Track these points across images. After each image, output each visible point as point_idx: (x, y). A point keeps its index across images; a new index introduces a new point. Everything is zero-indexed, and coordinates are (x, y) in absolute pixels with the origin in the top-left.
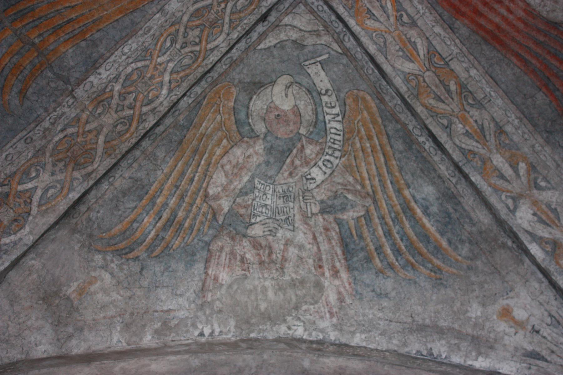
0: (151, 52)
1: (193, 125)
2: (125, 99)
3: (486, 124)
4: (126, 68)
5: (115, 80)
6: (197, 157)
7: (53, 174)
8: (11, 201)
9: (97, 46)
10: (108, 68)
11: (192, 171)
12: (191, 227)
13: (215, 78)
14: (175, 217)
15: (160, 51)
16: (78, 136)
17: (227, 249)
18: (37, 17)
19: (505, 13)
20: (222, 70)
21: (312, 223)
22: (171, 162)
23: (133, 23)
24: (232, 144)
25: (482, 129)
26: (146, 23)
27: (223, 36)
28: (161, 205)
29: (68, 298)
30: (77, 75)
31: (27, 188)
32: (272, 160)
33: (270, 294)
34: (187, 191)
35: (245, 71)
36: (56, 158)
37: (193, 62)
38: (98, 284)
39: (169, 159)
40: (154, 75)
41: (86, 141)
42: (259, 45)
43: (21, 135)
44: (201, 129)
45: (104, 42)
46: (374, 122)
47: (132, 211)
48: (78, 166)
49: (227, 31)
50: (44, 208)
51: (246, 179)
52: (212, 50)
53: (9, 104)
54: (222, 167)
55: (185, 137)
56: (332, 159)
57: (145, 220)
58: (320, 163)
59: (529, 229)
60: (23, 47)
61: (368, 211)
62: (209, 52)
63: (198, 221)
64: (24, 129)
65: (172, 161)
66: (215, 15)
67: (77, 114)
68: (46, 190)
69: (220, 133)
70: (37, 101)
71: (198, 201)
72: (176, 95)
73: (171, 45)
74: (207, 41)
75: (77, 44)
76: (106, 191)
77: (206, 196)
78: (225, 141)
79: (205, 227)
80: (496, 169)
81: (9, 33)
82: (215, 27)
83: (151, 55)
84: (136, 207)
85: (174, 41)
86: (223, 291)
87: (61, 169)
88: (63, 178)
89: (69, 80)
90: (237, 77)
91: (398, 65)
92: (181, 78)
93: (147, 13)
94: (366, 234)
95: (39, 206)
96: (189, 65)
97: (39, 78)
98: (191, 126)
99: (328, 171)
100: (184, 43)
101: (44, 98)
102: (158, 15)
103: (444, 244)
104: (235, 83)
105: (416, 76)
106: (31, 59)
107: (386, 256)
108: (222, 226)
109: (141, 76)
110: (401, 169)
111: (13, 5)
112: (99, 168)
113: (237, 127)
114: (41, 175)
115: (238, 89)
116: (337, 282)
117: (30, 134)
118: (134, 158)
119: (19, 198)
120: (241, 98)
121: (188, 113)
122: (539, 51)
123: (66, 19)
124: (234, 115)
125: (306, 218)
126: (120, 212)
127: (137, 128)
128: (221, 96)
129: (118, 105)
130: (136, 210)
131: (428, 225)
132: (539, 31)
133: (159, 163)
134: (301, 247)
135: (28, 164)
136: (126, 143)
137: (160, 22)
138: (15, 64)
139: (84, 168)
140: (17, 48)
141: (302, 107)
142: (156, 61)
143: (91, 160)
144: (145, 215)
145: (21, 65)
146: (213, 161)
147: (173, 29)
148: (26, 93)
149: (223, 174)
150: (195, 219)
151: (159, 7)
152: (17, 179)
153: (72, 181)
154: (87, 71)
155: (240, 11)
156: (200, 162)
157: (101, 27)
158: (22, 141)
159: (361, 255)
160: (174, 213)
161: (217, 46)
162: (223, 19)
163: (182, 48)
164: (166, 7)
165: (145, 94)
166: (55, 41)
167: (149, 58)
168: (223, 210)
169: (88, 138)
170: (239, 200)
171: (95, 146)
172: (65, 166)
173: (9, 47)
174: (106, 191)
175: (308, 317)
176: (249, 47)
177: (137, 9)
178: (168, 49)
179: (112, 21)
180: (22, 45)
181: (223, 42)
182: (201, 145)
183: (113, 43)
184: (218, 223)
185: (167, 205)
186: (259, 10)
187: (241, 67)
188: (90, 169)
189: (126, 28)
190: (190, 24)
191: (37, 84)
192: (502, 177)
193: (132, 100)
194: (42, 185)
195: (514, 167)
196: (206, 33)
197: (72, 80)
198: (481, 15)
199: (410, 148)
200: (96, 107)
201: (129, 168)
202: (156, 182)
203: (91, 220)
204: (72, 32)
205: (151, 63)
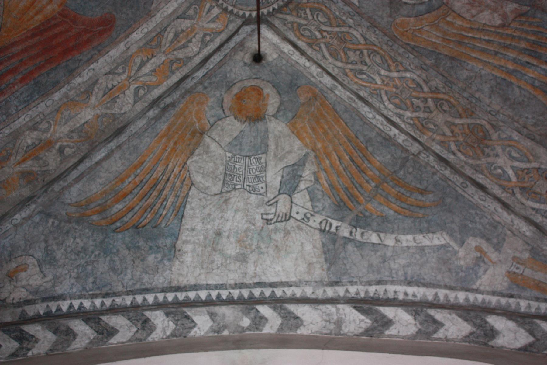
0: (373, 90)
1: (434, 50)
2: (418, 107)
4: (390, 110)
5: (402, 117)
6: (466, 41)
7: (497, 155)
8: (528, 184)
9: (370, 138)
10: (388, 129)
11: (479, 43)
12: (535, 33)
13: (388, 39)
14: (526, 49)
15: (371, 83)
16: (458, 141)
18: (352, 185)
20: (381, 33)
22: (472, 63)
23: (346, 110)
24: (450, 12)
26: (344, 101)
27: (351, 31)
28: (515, 65)
30: (399, 153)
31: (514, 174)
34: (500, 44)
35: (380, 13)
36: (481, 155)
37: (378, 53)
39: (469, 66)
40: (393, 85)
41: (462, 134)
42: (355, 4)
43: (460, 191)
44: (438, 42)
45: (366, 133)
47: (523, 89)
48: (486, 136)
49: (348, 28)
50: (531, 158)
52: (366, 39)
53: (434, 201)
54: (473, 16)
55: (446, 55)
57: (532, 75)
60: (380, 194)
62: (368, 42)
63: (529, 29)
64: (454, 189)
65: (470, 63)
66: (334, 39)
67: (437, 144)
68: (513, 158)
69: (441, 25)
70: (427, 181)
71: (509, 32)
72: (410, 65)
73: (365, 74)
74: (357, 45)
75: (371, 153)
76: (506, 116)
77: (503, 26)
78: (448, 19)
79: (534, 21)
81: (369, 206)
82: (345, 39)
83: (375, 89)
84: (519, 87)
85: (361, 72)
87: (492, 150)
88: (499, 147)
89: (404, 158)
90: (385, 20)
92: (394, 62)
93: (336, 100)
95: (529, 161)
96: (381, 57)
97: (406, 181)
98: (435, 52)
100: (362, 63)
101: (423, 176)
102: (337, 92)
104: (392, 20)
106: (390, 188)
109: (396, 96)
111: (345, 204)
112: (486, 119)
113: (434, 10)
114: (499, 165)
115: (397, 17)
117: (458, 184)
118: (470, 97)
119: (524, 179)
120: (405, 13)
121: (424, 57)
123: (351, 163)
124: (422, 15)
126: (525, 99)
127: (444, 93)
128: (405, 30)
129: (424, 112)
130: (522, 86)
133: (474, 74)
135: (490, 176)
136: (460, 100)
137: (342, 91)
138: (397, 199)
139: (487, 131)
140: (382, 198)
142: (380, 85)
143: (480, 127)
144: (526, 77)
145: (397, 195)
146: (468, 26)
147: (350, 74)
148: (422, 189)
149: (481, 14)
150: (527, 32)
151: (329, 92)
152: (506, 183)
153: (502, 139)
154: (394, 145)
155: (329, 19)
156: (471, 37)
157: (354, 136)
158: (466, 190)
160: (523, 52)
161: (362, 36)
162: (337, 32)
163: (366, 65)
164: (328, 86)
165: (411, 90)
166: (371, 170)
167: (378, 91)
168: (516, 8)
169: (459, 132)
171: (466, 126)
172: (488, 147)
173: (382, 205)
174: (506, 116)
176: (357, 13)
177: (333, 108)
178: (368, 76)
179: (346, 127)
180: (378, 195)
181: (357, 30)
182: (453, 39)
183: (366, 126)
184: (529, 10)
185: (514, 59)
186: (326, 3)
187: (376, 17)
188: (488, 127)
189: (351, 116)
190: (344, 60)
191: (412, 181)
193: (419, 101)
194: (509, 163)
196: (351, 46)
197: (404, 155)
200: (429, 129)
201: (480, 101)
202: (493, 73)
203: (535, 123)
204: (361, 158)
205: (383, 89)
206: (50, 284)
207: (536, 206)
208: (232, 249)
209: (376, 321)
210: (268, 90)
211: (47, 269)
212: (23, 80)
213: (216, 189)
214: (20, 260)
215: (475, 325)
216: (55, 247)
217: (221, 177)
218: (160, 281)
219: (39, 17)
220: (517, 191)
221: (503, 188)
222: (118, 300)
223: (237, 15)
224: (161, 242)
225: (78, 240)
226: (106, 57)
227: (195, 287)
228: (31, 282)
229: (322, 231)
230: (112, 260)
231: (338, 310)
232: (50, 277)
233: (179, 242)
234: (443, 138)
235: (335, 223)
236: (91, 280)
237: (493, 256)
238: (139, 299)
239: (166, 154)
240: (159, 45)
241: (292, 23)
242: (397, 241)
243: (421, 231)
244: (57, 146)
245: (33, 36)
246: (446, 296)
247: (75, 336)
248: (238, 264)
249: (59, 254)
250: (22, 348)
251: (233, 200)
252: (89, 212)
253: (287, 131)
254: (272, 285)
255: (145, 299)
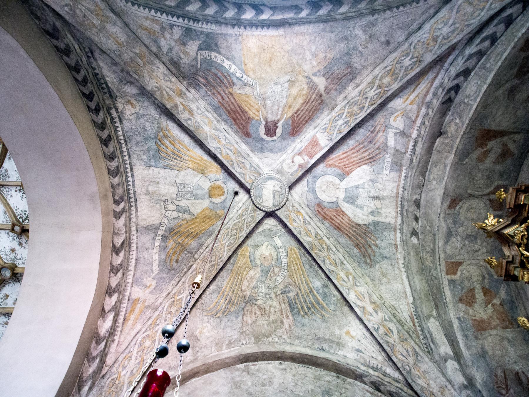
3: (337, 261)
12: (237, 303)
17: (250, 310)
19: (342, 220)
21: (278, 298)
25: (336, 262)
27: (244, 231)
29: (196, 336)
32: (263, 275)
33: (265, 326)
38: (206, 329)
46: (298, 258)
51: (255, 283)
56: (284, 273)
58: (280, 275)
59: (354, 302)
61: (297, 293)
80: (341, 277)
85: (227, 235)
86: (249, 326)
91: (305, 238)
94: (298, 302)
99: (283, 278)
103: (325, 305)
105: (312, 242)
107: (305, 310)
108: (247, 302)
110: (308, 276)
116: (288, 321)
122: (354, 234)
125: (276, 296)
131: (319, 298)
132: (353, 226)
134: (275, 307)
141: (272, 254)
159: (296, 310)
170: (253, 291)
175: (279, 334)
192: (344, 281)
195: (348, 277)
198: (333, 220)
199: (311, 267)
206: (127, 118)
207: (166, 308)
208: (151, 189)
209: (118, 249)
210: (223, 198)
211: (134, 116)
212: (220, 102)
213: (178, 181)
214: (137, 104)
215: (115, 288)
216: (145, 118)
217: (184, 182)
218: (134, 161)
219: (247, 109)
220: (173, 299)
221: (175, 294)
222: (124, 145)
223: (251, 187)
224: (153, 160)
225: (150, 128)
226: (234, 134)
227: (133, 176)
228: (127, 110)
229: (160, 224)
230: (142, 142)
231: (123, 234)
232: (131, 118)
233: (153, 168)
234: (198, 268)
235: (164, 228)
236: (131, 134)
237: (148, 291)
238: (126, 154)
239: (193, 160)
240: (238, 156)
241: (248, 208)
242: (155, 253)
243: (159, 262)
244: (191, 118)
245: (239, 107)
246: (130, 275)
247: (102, 131)
248: (145, 191)
249: (142, 120)
250: (92, 110)
251: (173, 187)
252: (164, 131)
253: (204, 207)
254: (136, 206)
255: (125, 156)
